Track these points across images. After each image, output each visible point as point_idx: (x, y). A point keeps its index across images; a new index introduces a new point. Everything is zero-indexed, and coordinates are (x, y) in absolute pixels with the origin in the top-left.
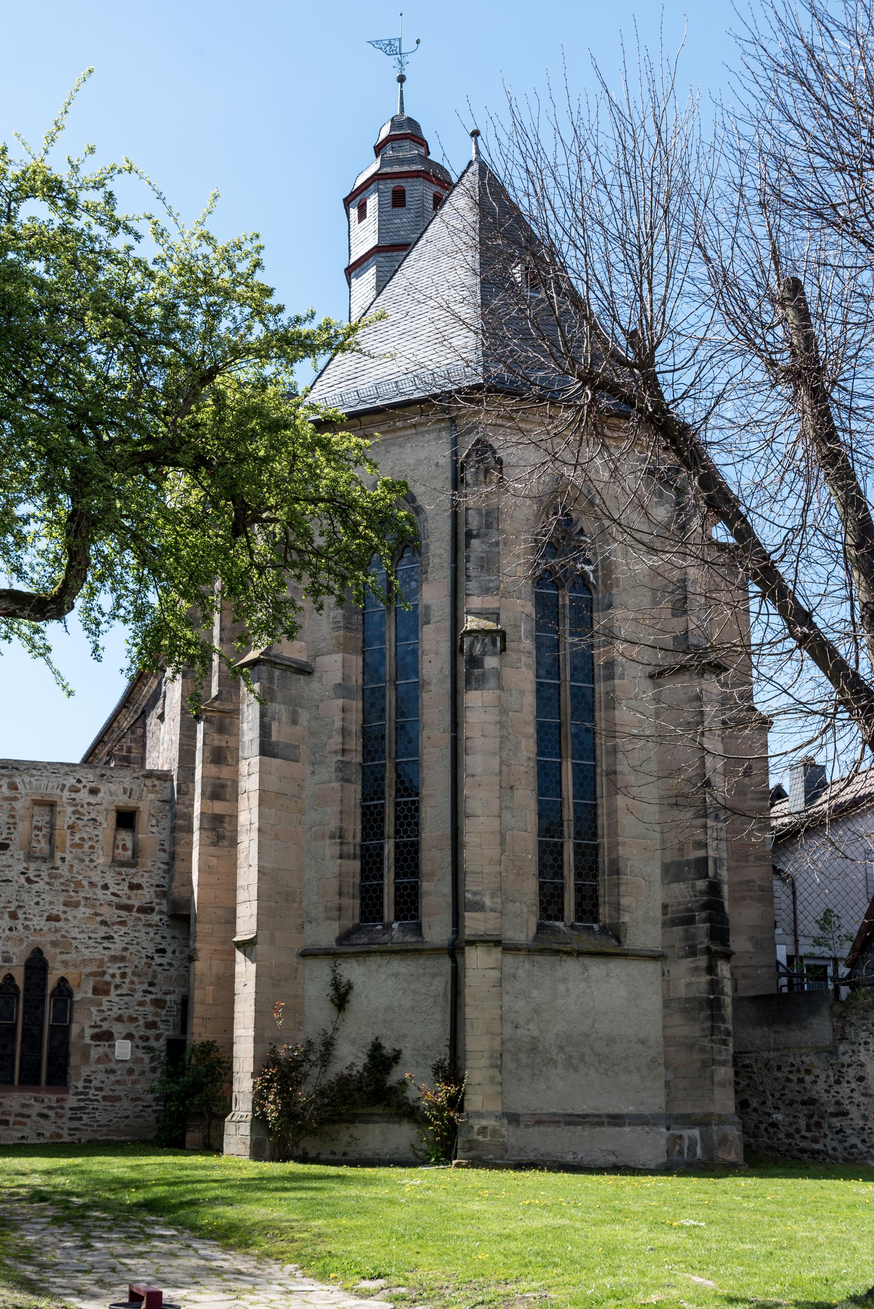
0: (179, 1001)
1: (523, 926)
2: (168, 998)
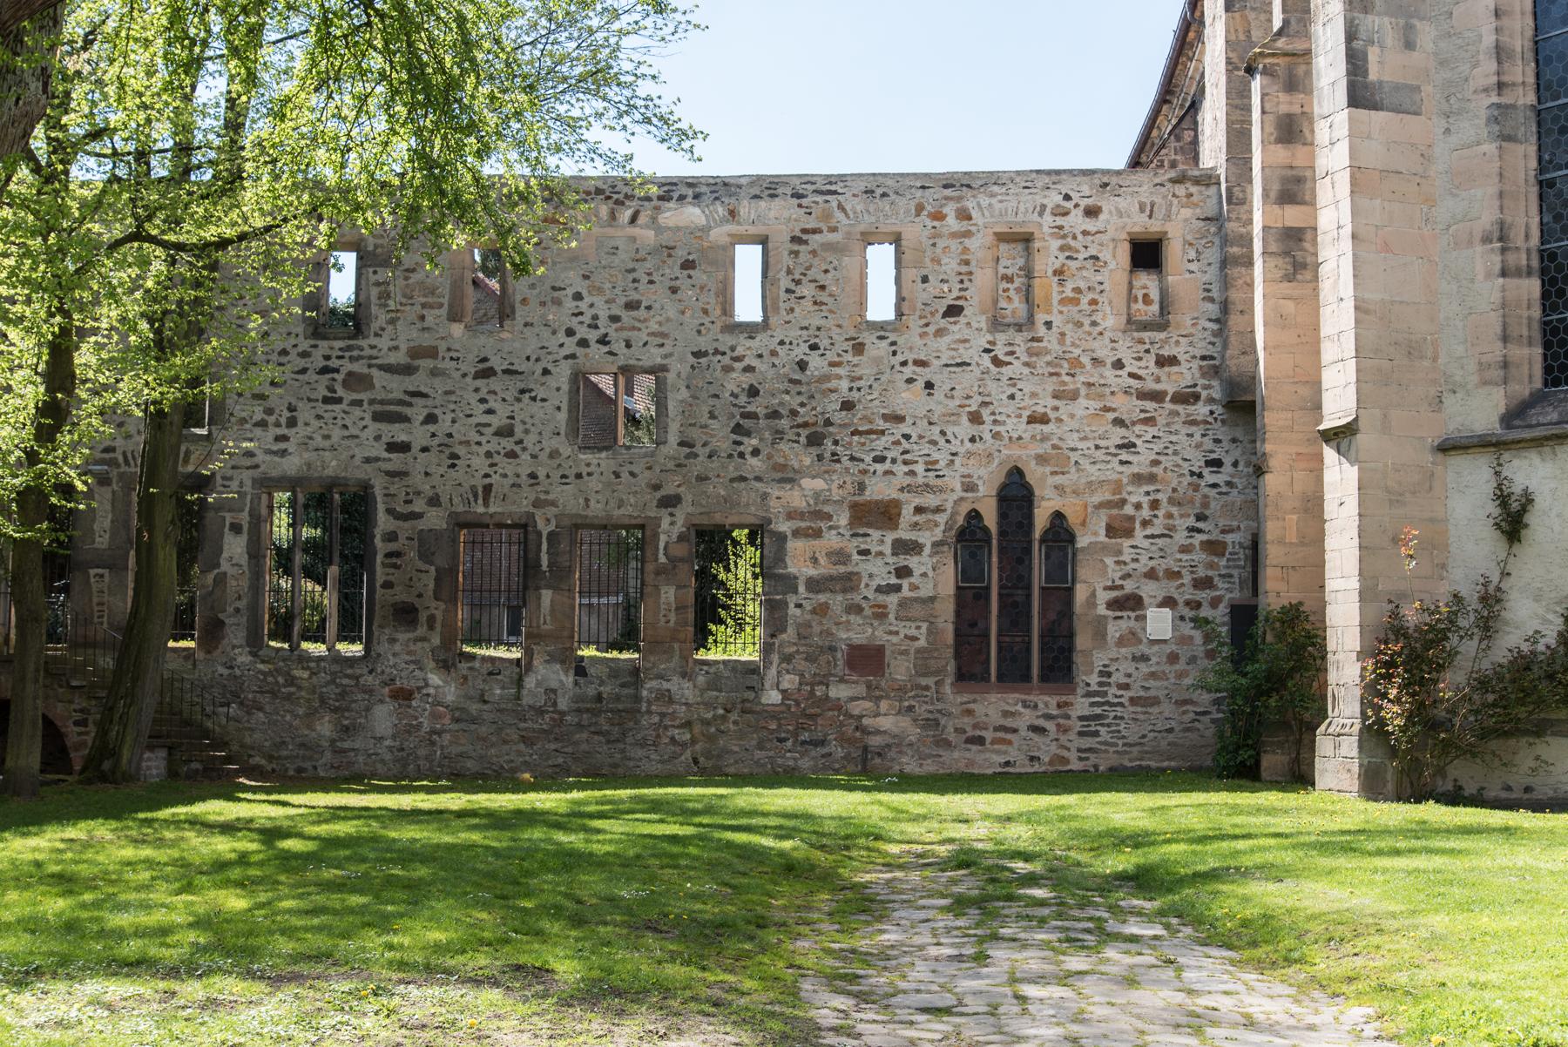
0: (1248, 543)
2: (1229, 538)
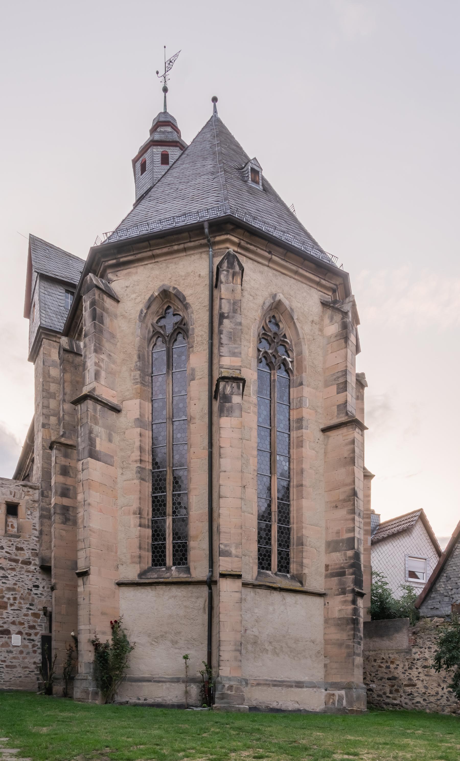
1: (251, 572)
